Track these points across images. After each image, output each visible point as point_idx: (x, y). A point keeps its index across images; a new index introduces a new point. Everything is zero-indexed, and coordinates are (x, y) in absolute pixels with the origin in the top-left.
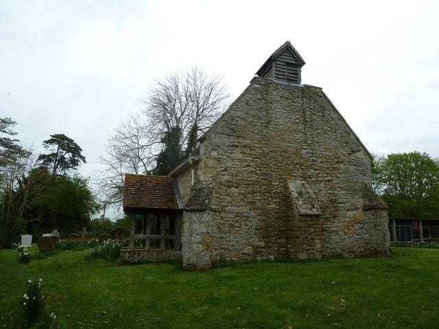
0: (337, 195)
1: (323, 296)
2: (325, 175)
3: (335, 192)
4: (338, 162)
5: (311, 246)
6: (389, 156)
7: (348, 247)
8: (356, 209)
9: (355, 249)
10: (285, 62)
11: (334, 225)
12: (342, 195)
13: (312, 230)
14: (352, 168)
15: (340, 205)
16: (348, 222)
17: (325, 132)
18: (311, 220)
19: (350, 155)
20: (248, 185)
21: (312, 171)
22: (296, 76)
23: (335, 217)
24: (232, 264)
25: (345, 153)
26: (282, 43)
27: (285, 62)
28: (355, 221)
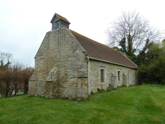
0: (67, 72)
1: (55, 112)
2: (64, 64)
3: (67, 71)
4: (68, 57)
5: (49, 93)
6: (149, 45)
7: (70, 95)
8: (75, 77)
9: (73, 96)
10: (59, 22)
11: (65, 85)
12: (70, 72)
13: (50, 87)
14: (74, 59)
15: (68, 76)
16: (71, 84)
17: (65, 45)
18: (50, 83)
19: (73, 52)
20: (43, 71)
21: (60, 63)
22: (67, 27)
23: (66, 81)
24: (83, 100)
25: (71, 52)
26: (53, 15)
27: (59, 22)
28: (73, 83)
